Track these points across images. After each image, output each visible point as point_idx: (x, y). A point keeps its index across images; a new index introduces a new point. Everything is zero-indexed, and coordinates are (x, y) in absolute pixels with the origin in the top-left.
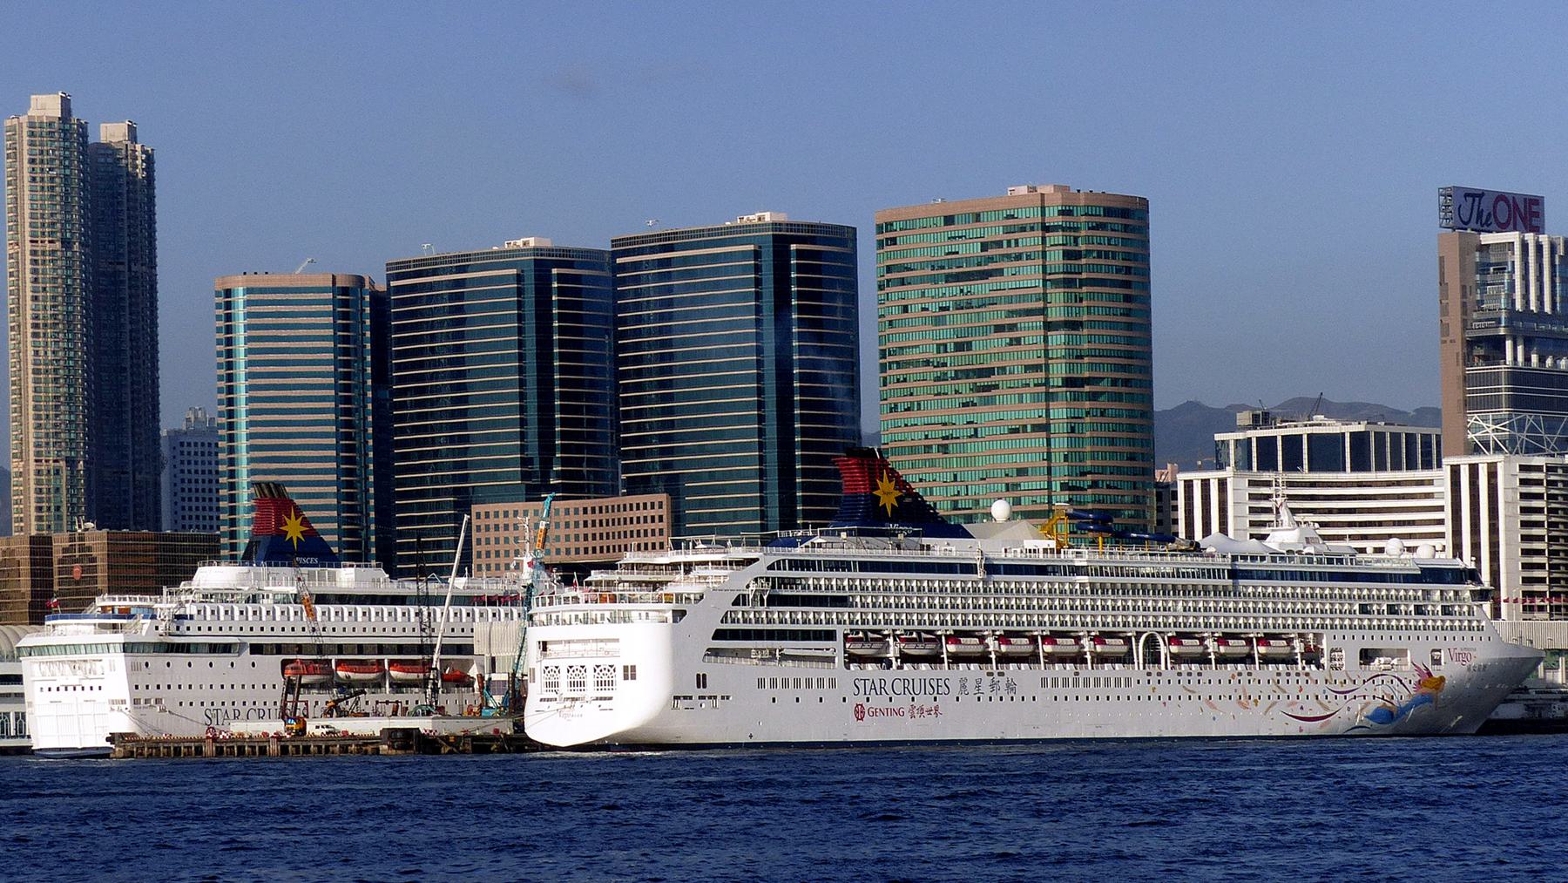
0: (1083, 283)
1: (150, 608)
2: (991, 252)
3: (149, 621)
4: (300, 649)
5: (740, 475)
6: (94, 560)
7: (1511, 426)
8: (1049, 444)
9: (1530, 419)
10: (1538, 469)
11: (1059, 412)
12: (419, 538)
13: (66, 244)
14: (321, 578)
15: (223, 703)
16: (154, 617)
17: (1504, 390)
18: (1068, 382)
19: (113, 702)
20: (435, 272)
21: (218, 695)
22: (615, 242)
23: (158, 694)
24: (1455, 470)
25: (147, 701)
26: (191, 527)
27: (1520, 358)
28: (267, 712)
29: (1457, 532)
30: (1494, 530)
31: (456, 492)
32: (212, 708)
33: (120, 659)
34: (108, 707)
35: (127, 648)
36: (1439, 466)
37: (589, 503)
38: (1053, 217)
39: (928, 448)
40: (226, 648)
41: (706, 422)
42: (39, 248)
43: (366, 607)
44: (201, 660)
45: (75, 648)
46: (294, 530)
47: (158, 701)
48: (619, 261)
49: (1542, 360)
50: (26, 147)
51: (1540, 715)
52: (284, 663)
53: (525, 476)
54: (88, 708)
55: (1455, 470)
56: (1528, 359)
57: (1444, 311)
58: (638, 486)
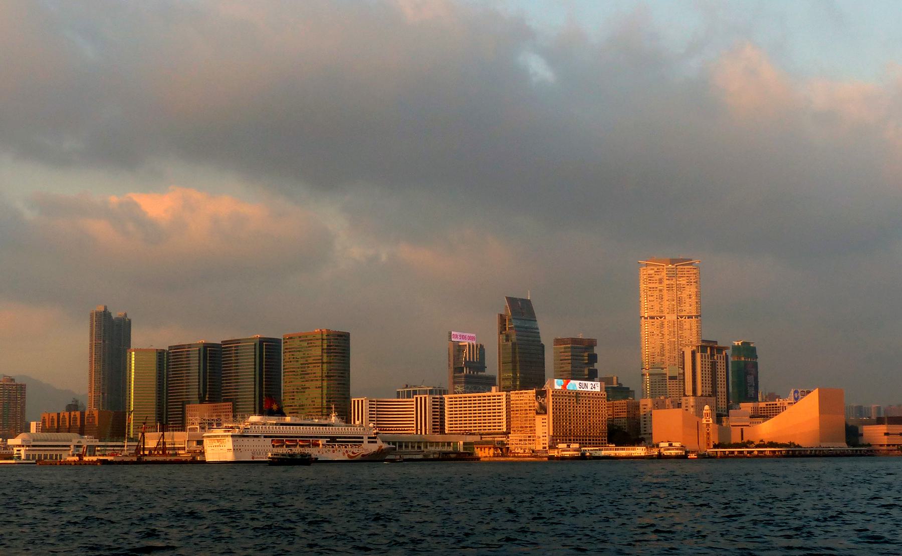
0: (331, 353)
1: (238, 426)
2: (309, 345)
6: (95, 417)
7: (465, 388)
8: (322, 391)
9: (470, 387)
10: (437, 398)
11: (325, 383)
13: (104, 341)
14: (282, 419)
16: (239, 429)
17: (463, 380)
18: (327, 376)
19: (228, 450)
21: (255, 448)
22: (222, 342)
23: (240, 448)
24: (417, 398)
25: (237, 449)
26: (192, 407)
27: (468, 372)
29: (417, 417)
33: (230, 439)
35: (232, 436)
36: (413, 398)
37: (216, 404)
38: (325, 337)
39: (294, 392)
40: (257, 436)
42: (97, 342)
43: (306, 427)
44: (251, 440)
45: (219, 436)
47: (240, 449)
49: (473, 373)
50: (94, 318)
52: (272, 440)
53: (199, 398)
54: (221, 451)
55: (417, 398)
56: (470, 372)
57: (449, 361)
58: (226, 401)
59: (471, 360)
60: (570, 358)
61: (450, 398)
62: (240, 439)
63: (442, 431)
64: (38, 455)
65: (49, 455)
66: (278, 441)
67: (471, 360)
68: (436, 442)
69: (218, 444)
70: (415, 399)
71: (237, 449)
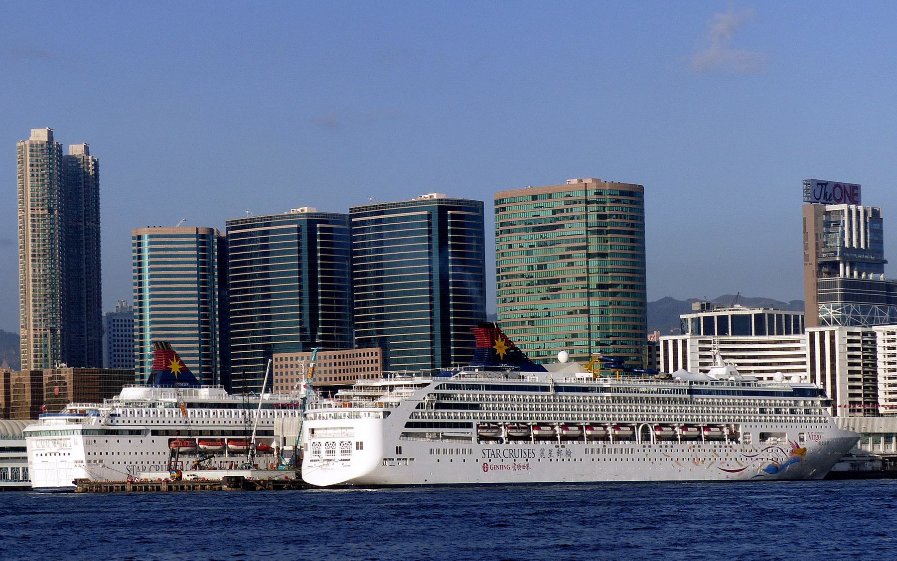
1: (96, 410)
2: (557, 215)
3: (96, 417)
4: (179, 433)
5: (420, 337)
7: (842, 311)
9: (853, 307)
10: (857, 334)
11: (595, 303)
12: (244, 372)
14: (190, 394)
15: (137, 463)
16: (98, 415)
17: (839, 291)
19: (76, 462)
20: (253, 226)
21: (134, 460)
23: (101, 457)
24: (812, 335)
26: (119, 366)
27: (848, 273)
28: (161, 467)
30: (833, 367)
31: (264, 346)
32: (130, 465)
33: (80, 438)
34: (73, 464)
35: (84, 432)
36: (803, 332)
37: (337, 353)
38: (592, 196)
40: (138, 432)
41: (396, 309)
43: (215, 410)
44: (124, 439)
45: (56, 432)
46: (175, 367)
47: (101, 461)
48: (354, 220)
49: (860, 274)
51: (858, 469)
52: (170, 441)
55: (812, 335)
56: (852, 274)
57: (806, 247)
59: (855, 245)
60: (195, 272)
61: (888, 334)
62: (102, 439)
63: (873, 410)
64: (12, 469)
65: (9, 470)
66: (184, 443)
67: (855, 245)
68: (874, 434)
69: (54, 450)
70: (807, 336)
71: (95, 461)
